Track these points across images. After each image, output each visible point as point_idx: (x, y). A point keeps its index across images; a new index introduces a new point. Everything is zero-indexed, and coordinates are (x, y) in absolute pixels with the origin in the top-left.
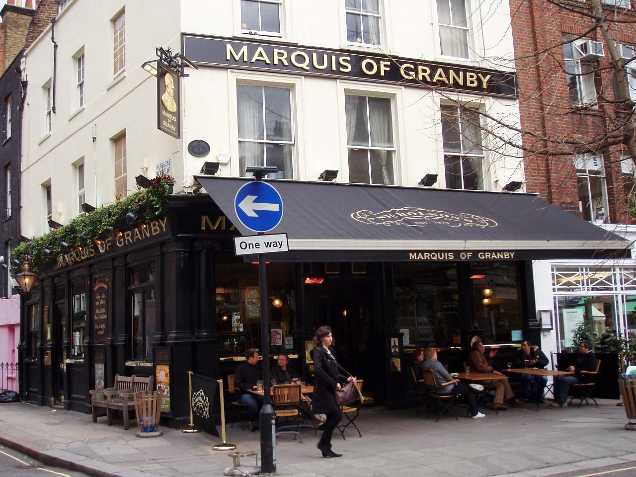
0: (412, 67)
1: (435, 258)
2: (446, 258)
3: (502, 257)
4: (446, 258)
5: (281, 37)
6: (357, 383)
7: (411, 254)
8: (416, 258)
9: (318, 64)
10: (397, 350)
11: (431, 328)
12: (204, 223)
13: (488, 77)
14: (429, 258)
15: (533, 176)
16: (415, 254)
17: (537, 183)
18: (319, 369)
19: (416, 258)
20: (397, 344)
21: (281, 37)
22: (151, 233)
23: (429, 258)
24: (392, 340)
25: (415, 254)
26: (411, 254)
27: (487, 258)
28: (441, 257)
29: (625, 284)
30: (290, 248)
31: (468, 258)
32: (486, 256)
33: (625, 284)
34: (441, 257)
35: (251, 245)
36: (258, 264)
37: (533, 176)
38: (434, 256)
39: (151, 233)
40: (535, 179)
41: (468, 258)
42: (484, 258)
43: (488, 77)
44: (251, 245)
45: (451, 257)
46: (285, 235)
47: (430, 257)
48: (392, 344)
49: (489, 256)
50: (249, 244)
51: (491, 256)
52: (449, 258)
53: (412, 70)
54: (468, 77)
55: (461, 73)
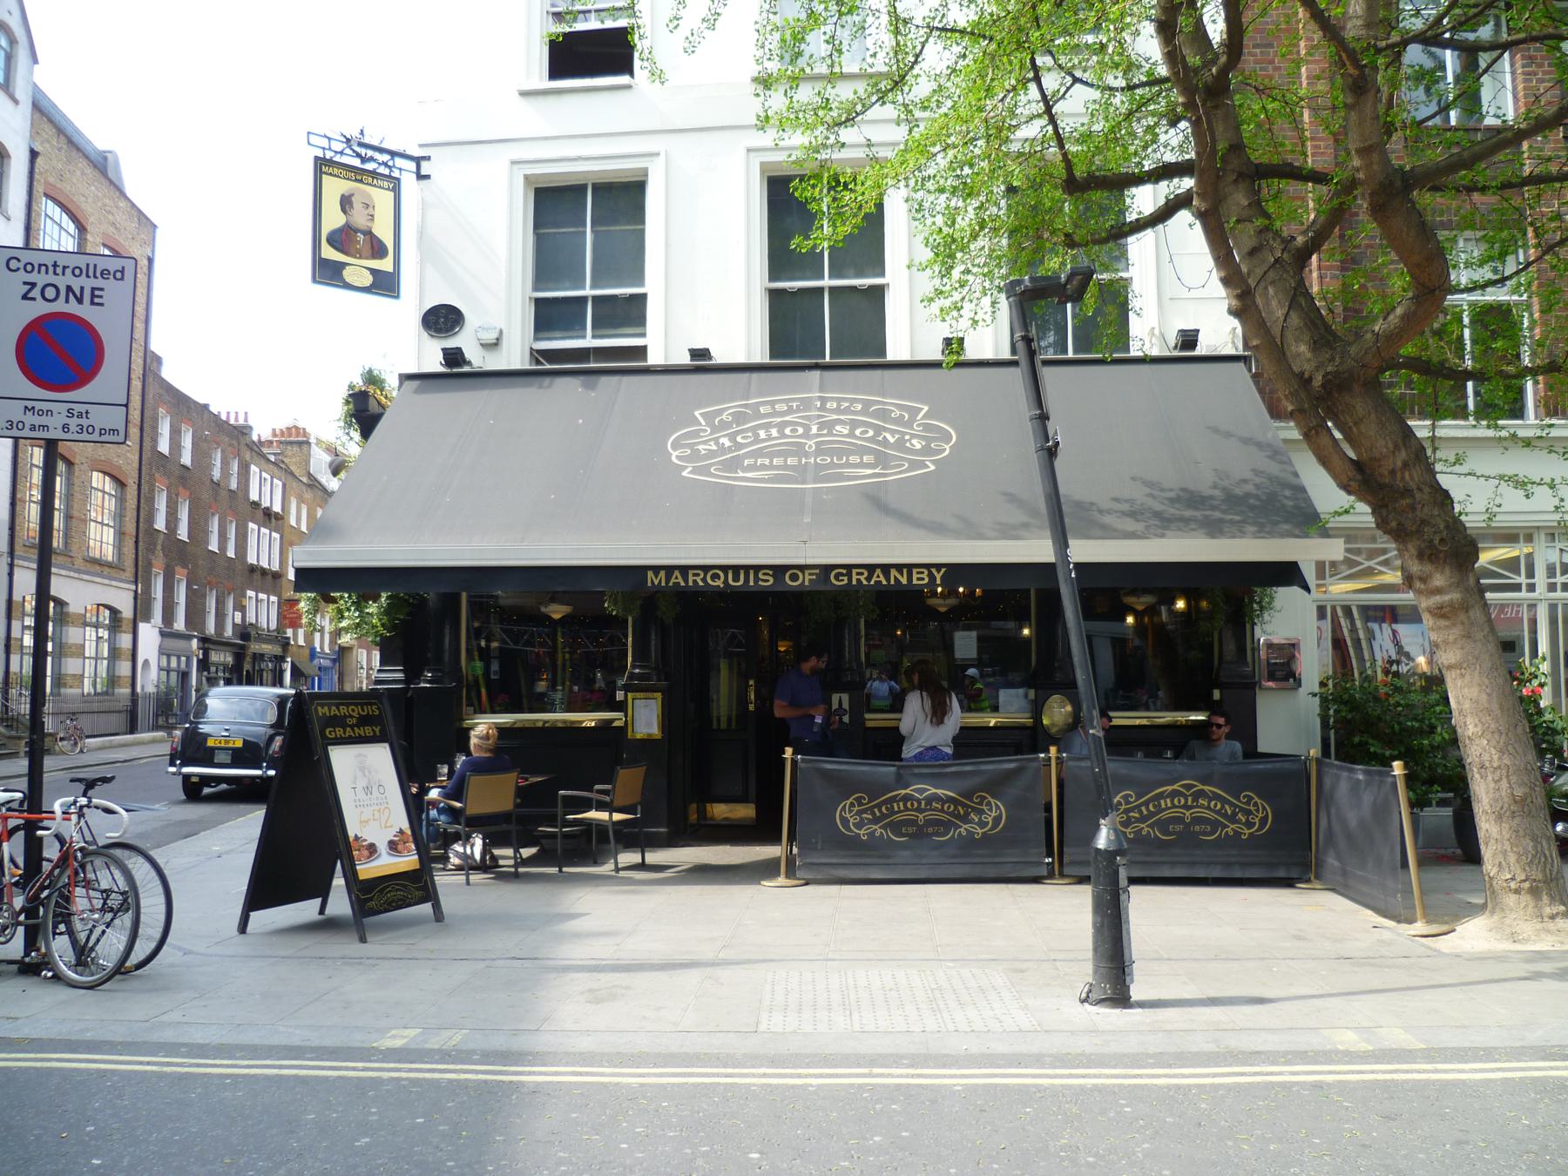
0: (844, 571)
1: (719, 583)
2: (752, 583)
3: (904, 581)
4: (752, 583)
7: (650, 574)
8: (663, 584)
9: (733, 581)
10: (846, 719)
11: (1394, 546)
12: (649, 581)
13: (943, 570)
14: (701, 584)
16: (662, 574)
19: (663, 584)
23: (701, 584)
26: (650, 574)
27: (854, 582)
28: (363, 711)
30: (82, 630)
31: (807, 583)
32: (855, 577)
34: (363, 711)
35: (43, 268)
36: (469, 597)
41: (807, 583)
42: (846, 582)
43: (943, 570)
44: (43, 268)
45: (768, 581)
47: (704, 580)
49: (862, 578)
50: (40, 265)
52: (760, 583)
53: (842, 574)
54: (854, 574)
55: (905, 571)
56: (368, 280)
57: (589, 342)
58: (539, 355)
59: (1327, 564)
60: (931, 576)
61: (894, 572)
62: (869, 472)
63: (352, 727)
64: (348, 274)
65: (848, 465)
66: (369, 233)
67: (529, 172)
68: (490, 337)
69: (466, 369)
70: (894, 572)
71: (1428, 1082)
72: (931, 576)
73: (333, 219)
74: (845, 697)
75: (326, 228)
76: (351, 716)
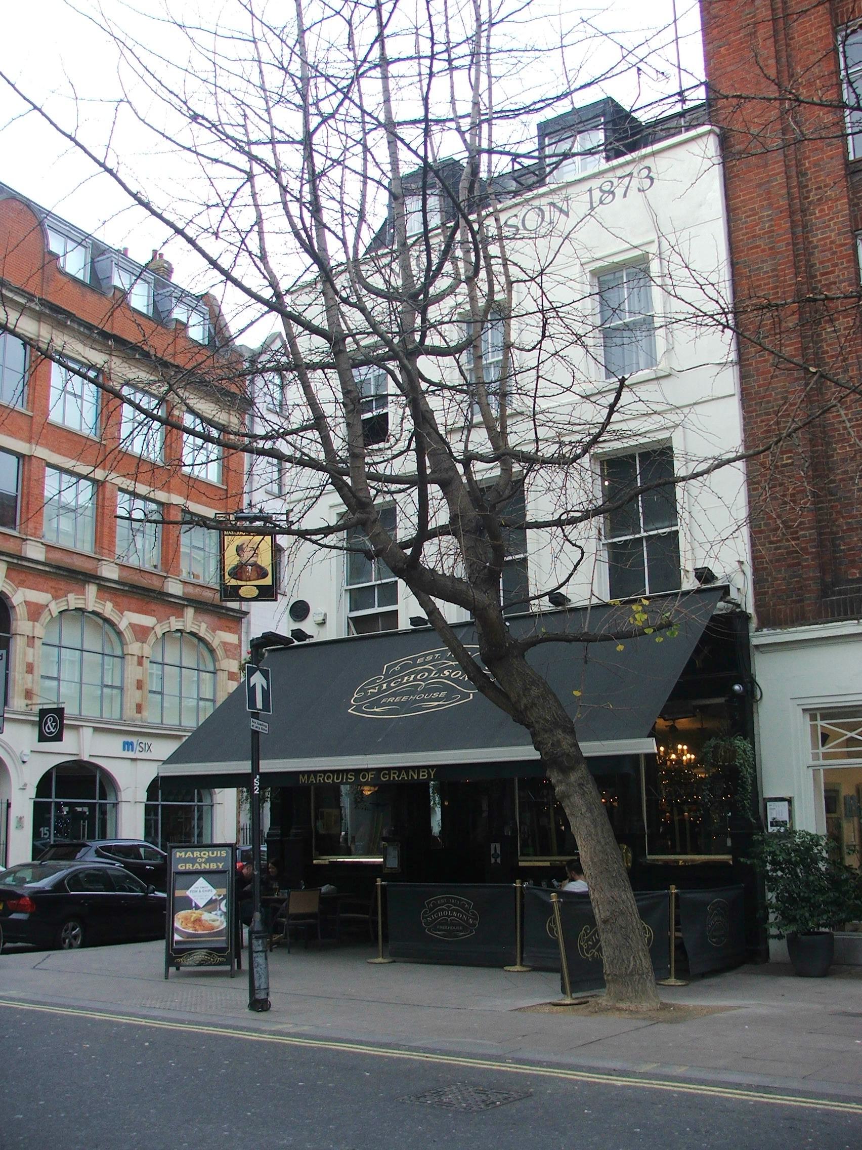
5: (625, 196)
6: (521, 965)
7: (301, 777)
10: (499, 860)
15: (771, 542)
17: (782, 554)
18: (252, 422)
20: (498, 852)
21: (625, 196)
22: (418, 776)
24: (493, 846)
25: (306, 777)
28: (338, 779)
29: (823, 746)
33: (823, 746)
37: (771, 542)
38: (329, 778)
39: (418, 776)
40: (777, 548)
46: (786, 803)
48: (493, 852)
51: (398, 777)
56: (255, 592)
57: (377, 610)
58: (357, 622)
59: (642, 760)
60: (429, 774)
61: (411, 772)
62: (437, 703)
63: (200, 864)
64: (243, 592)
65: (424, 700)
66: (255, 565)
67: (338, 511)
68: (320, 619)
69: (307, 641)
70: (411, 772)
71: (248, 1039)
72: (429, 774)
73: (232, 559)
74: (498, 846)
75: (228, 568)
76: (202, 858)
